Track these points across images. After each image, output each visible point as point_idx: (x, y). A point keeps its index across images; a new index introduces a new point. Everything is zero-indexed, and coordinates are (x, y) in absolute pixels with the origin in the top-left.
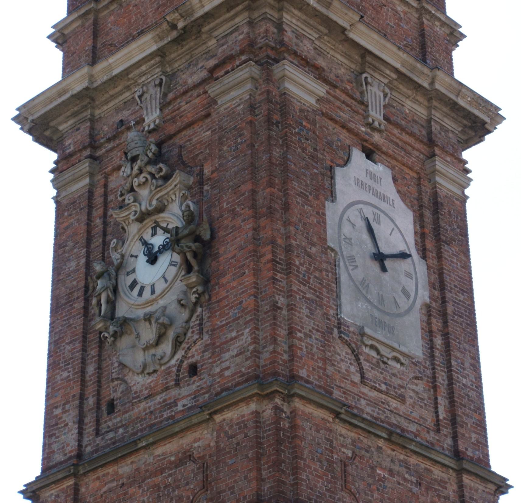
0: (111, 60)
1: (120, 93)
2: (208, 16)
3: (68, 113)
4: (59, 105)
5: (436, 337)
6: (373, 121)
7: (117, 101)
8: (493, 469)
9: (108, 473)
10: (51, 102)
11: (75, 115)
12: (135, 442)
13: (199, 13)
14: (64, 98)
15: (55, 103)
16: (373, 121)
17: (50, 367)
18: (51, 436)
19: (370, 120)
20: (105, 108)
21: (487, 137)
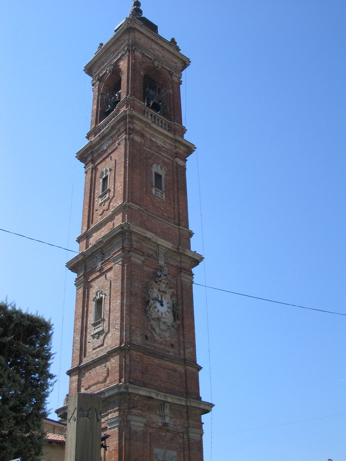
0: (160, 239)
1: (152, 246)
2: (186, 255)
3: (138, 237)
4: (140, 234)
5: (184, 372)
6: (161, 264)
7: (149, 246)
8: (197, 363)
9: (151, 359)
10: (139, 231)
11: (139, 238)
12: (164, 357)
13: (186, 253)
14: (143, 234)
15: (139, 233)
16: (161, 264)
17: (193, 354)
18: (194, 355)
19: (160, 264)
20: (145, 244)
21: (200, 263)
